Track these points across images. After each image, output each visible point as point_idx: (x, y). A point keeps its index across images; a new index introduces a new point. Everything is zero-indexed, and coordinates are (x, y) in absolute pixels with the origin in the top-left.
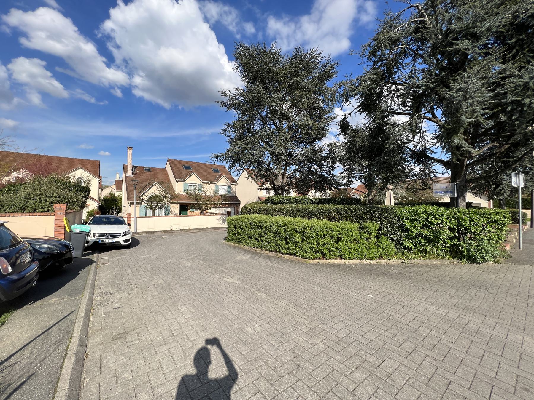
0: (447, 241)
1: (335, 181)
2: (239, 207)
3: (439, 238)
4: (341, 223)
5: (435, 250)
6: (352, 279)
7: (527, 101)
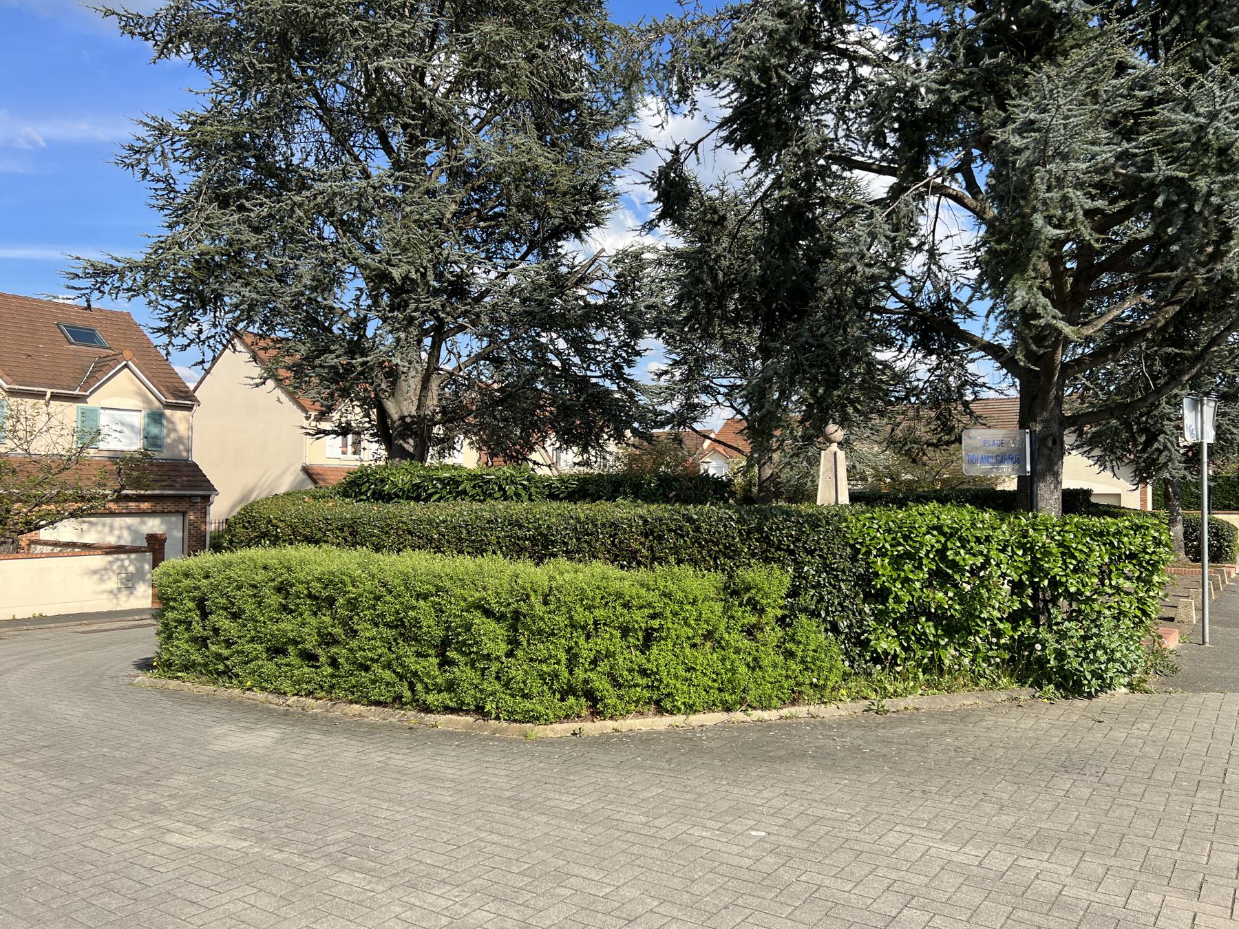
0: (1001, 626)
1: (638, 407)
2: (204, 513)
3: (979, 617)
4: (659, 575)
5: (966, 661)
6: (696, 782)
7: (1202, 183)
